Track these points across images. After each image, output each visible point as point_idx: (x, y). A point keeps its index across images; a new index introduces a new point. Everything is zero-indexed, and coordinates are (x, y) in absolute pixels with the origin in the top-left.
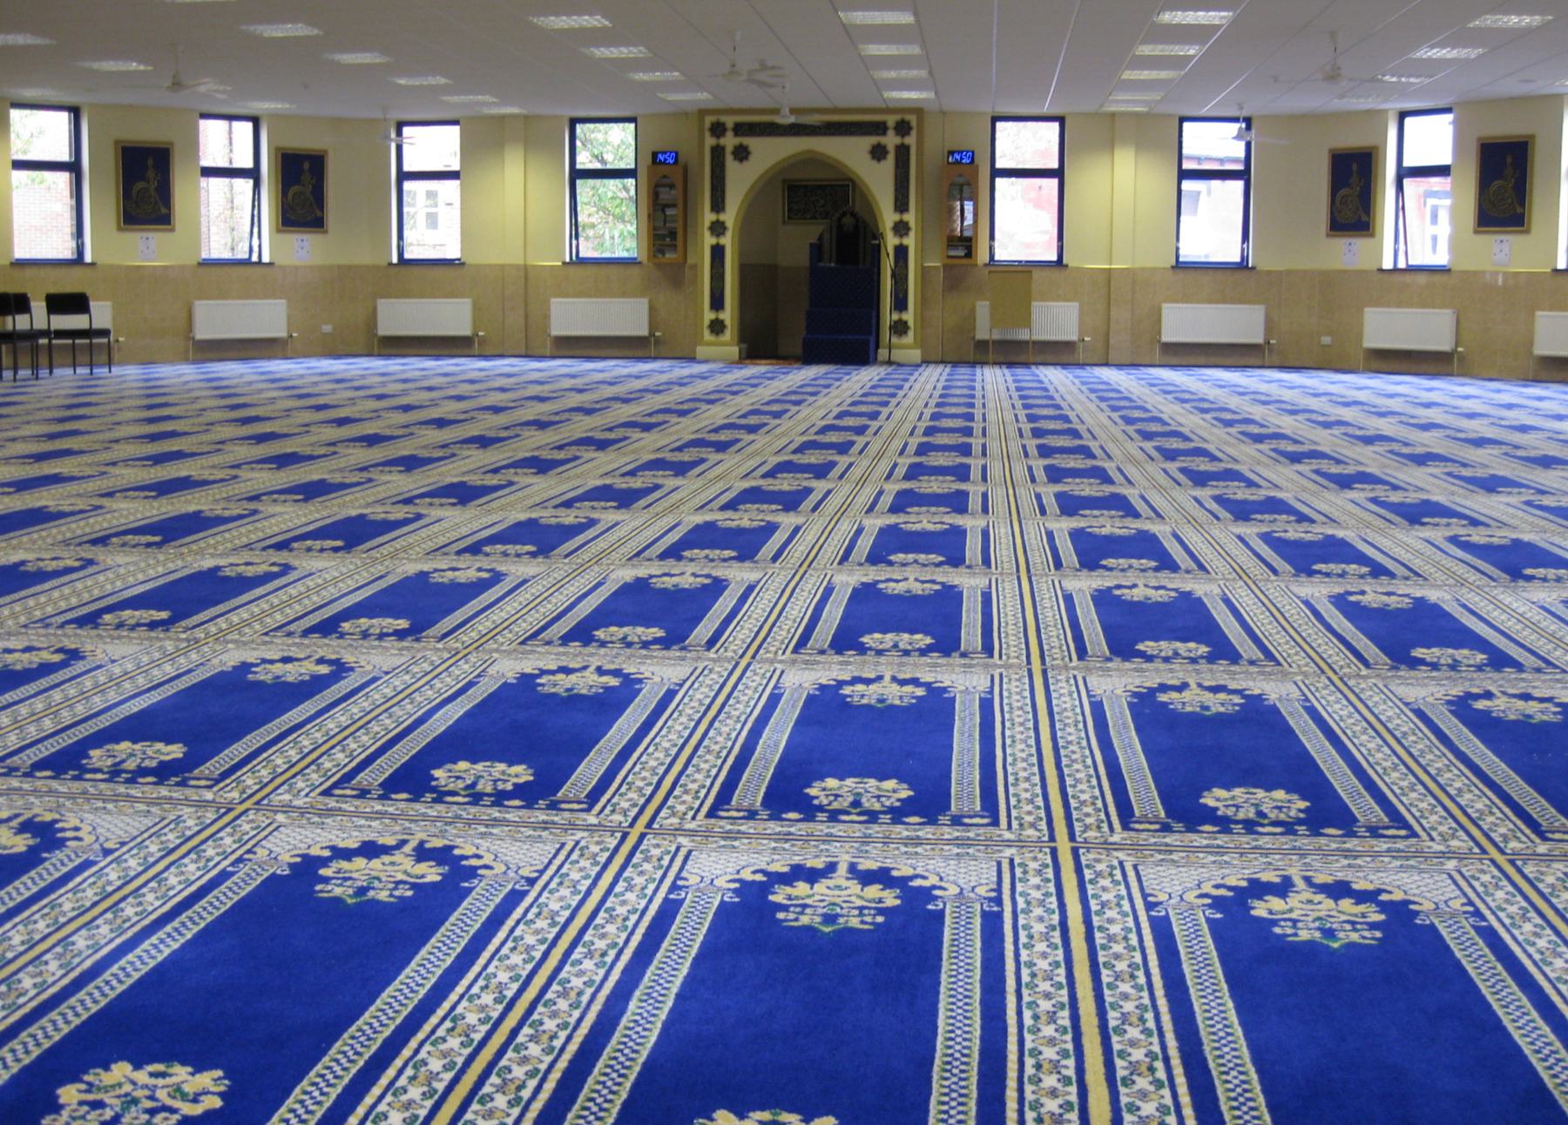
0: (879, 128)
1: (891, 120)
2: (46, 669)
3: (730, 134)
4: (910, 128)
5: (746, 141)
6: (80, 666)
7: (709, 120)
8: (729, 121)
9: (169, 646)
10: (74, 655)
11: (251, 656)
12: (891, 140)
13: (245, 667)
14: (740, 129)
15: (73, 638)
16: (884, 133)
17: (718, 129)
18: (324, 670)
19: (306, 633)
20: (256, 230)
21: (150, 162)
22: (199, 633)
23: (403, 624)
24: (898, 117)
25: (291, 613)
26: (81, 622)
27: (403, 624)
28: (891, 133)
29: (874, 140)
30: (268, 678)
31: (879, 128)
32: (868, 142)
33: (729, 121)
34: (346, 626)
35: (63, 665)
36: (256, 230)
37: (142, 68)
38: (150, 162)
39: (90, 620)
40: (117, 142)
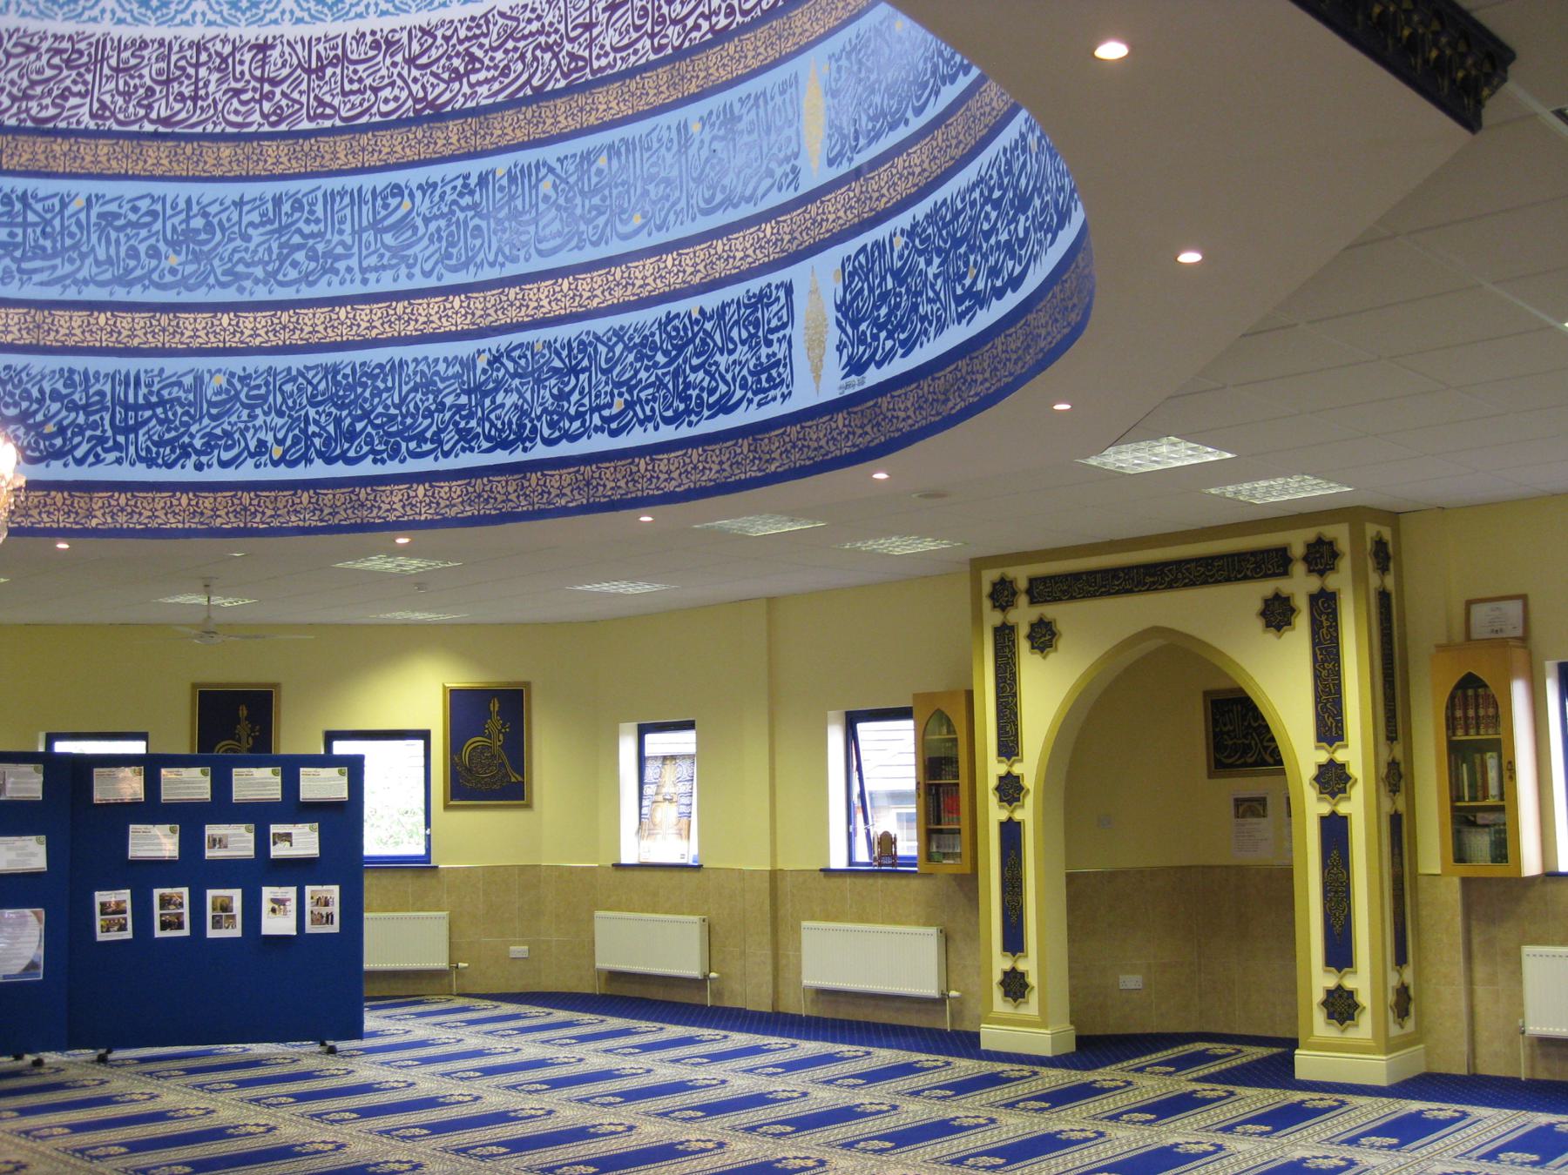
0: (1275, 562)
1: (1297, 541)
2: (1206, 1154)
3: (1314, 584)
4: (1335, 555)
5: (1050, 611)
6: (1222, 1154)
7: (989, 576)
8: (1021, 575)
9: (1268, 1146)
10: (1220, 1148)
11: (1307, 1154)
12: (1299, 585)
13: (1304, 1160)
14: (1042, 590)
15: (1219, 1138)
16: (1032, 581)
17: (1003, 594)
18: (1343, 1163)
19: (1480, 1158)
20: (855, 775)
21: (243, 712)
22: (1284, 1140)
23: (1535, 1158)
24: (1310, 534)
25: (1469, 1146)
26: (1111, 1118)
27: (1535, 1158)
28: (1299, 569)
29: (1267, 587)
30: (1312, 1166)
31: (1275, 562)
32: (1255, 592)
33: (1021, 575)
34: (1502, 1156)
35: (1215, 1152)
36: (855, 775)
37: (1230, 490)
38: (243, 712)
39: (1229, 1129)
40: (277, 685)
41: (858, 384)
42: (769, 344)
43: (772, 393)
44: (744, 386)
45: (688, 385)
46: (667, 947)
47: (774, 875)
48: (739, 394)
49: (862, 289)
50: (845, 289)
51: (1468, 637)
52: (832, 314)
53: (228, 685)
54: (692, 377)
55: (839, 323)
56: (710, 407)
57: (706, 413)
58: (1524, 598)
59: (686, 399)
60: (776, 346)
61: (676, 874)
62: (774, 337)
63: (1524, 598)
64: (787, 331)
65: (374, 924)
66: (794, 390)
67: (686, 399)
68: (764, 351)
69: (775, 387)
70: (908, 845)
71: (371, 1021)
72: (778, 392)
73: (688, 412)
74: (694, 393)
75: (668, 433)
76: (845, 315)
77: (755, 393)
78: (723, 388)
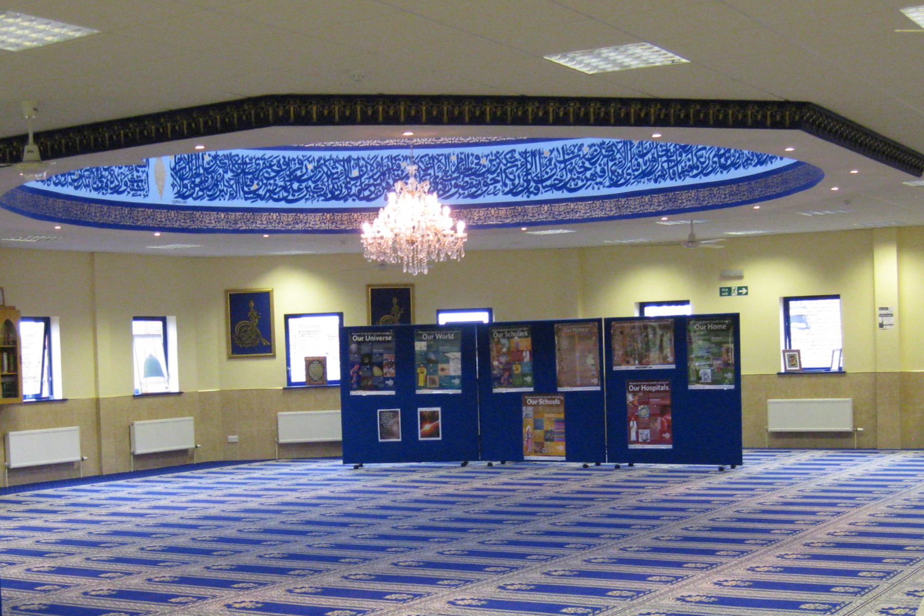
21: (395, 300)
38: (395, 300)
41: (181, 202)
42: (138, 171)
43: (139, 193)
44: (126, 185)
45: (102, 176)
46: (174, 434)
47: (97, 401)
48: (123, 188)
49: (185, 168)
50: (176, 164)
51: (164, 320)
52: (169, 172)
53: (397, 285)
54: (104, 173)
55: (172, 176)
56: (111, 189)
57: (109, 191)
58: (786, 301)
59: (101, 182)
60: (140, 174)
61: (162, 399)
62: (140, 169)
63: (786, 301)
64: (146, 169)
65: (530, 408)
66: (149, 194)
67: (101, 182)
68: (135, 174)
69: (140, 190)
70: (334, 372)
71: (526, 458)
72: (142, 193)
73: (102, 188)
74: (105, 180)
75: (94, 195)
76: (176, 173)
77: (132, 190)
78: (116, 183)
